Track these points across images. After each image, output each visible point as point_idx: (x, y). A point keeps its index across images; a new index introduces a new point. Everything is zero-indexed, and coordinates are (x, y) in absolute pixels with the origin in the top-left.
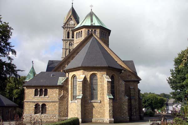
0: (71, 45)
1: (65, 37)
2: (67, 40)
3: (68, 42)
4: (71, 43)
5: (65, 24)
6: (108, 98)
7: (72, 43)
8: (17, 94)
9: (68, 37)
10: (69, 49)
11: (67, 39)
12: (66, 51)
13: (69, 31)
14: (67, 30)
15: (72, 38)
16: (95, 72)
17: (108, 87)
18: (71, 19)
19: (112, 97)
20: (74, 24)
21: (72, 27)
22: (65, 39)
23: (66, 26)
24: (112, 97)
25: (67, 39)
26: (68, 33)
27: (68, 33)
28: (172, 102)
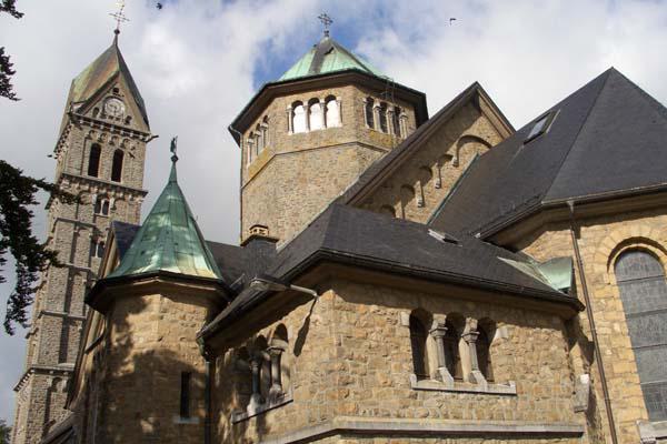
0: (105, 212)
1: (77, 163)
2: (88, 181)
3: (89, 191)
4: (107, 204)
5: (87, 104)
6: (320, 298)
7: (112, 201)
8: (127, 363)
9: (93, 170)
10: (95, 228)
11: (85, 175)
12: (76, 235)
13: (100, 140)
14: (89, 138)
15: (113, 179)
16: (213, 322)
17: (560, 274)
18: (116, 90)
19: (400, 204)
20: (129, 118)
21: (120, 128)
22: (75, 172)
23: (89, 115)
24: (400, 204)
25: (85, 175)
26: (96, 152)
27: (96, 152)
28: (156, 301)
